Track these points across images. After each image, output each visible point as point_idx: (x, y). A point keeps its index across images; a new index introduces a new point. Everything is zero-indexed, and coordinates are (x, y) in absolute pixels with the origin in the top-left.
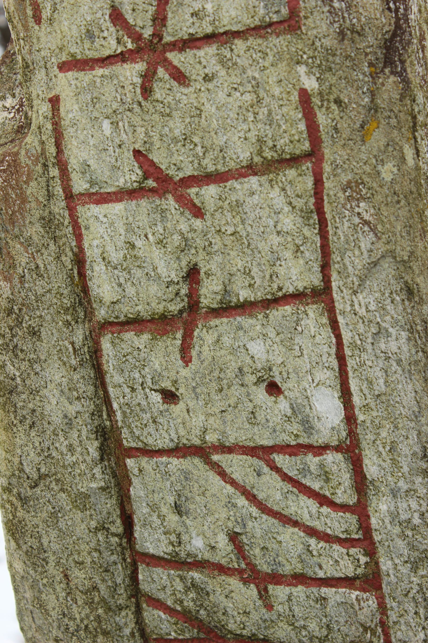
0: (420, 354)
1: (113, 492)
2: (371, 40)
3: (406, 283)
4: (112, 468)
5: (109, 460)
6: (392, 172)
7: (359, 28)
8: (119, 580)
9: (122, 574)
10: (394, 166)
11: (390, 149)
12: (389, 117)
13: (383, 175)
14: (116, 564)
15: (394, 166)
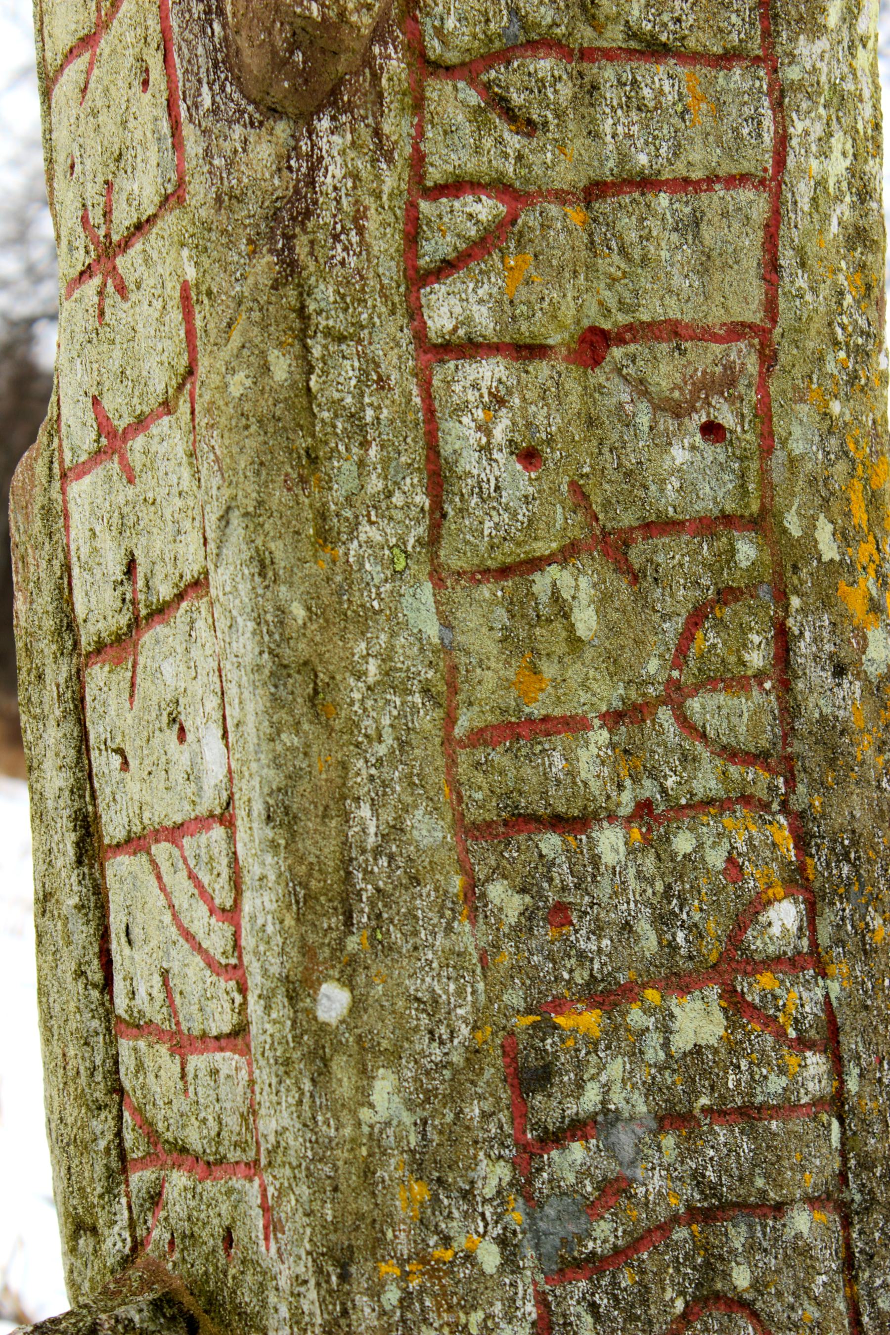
0: (266, 656)
1: (91, 916)
2: (253, 208)
3: (257, 550)
4: (95, 880)
5: (91, 867)
6: (243, 384)
7: (238, 192)
8: (98, 1062)
9: (102, 1051)
10: (247, 377)
11: (246, 352)
12: (251, 309)
13: (231, 388)
14: (97, 1034)
15: (247, 377)
